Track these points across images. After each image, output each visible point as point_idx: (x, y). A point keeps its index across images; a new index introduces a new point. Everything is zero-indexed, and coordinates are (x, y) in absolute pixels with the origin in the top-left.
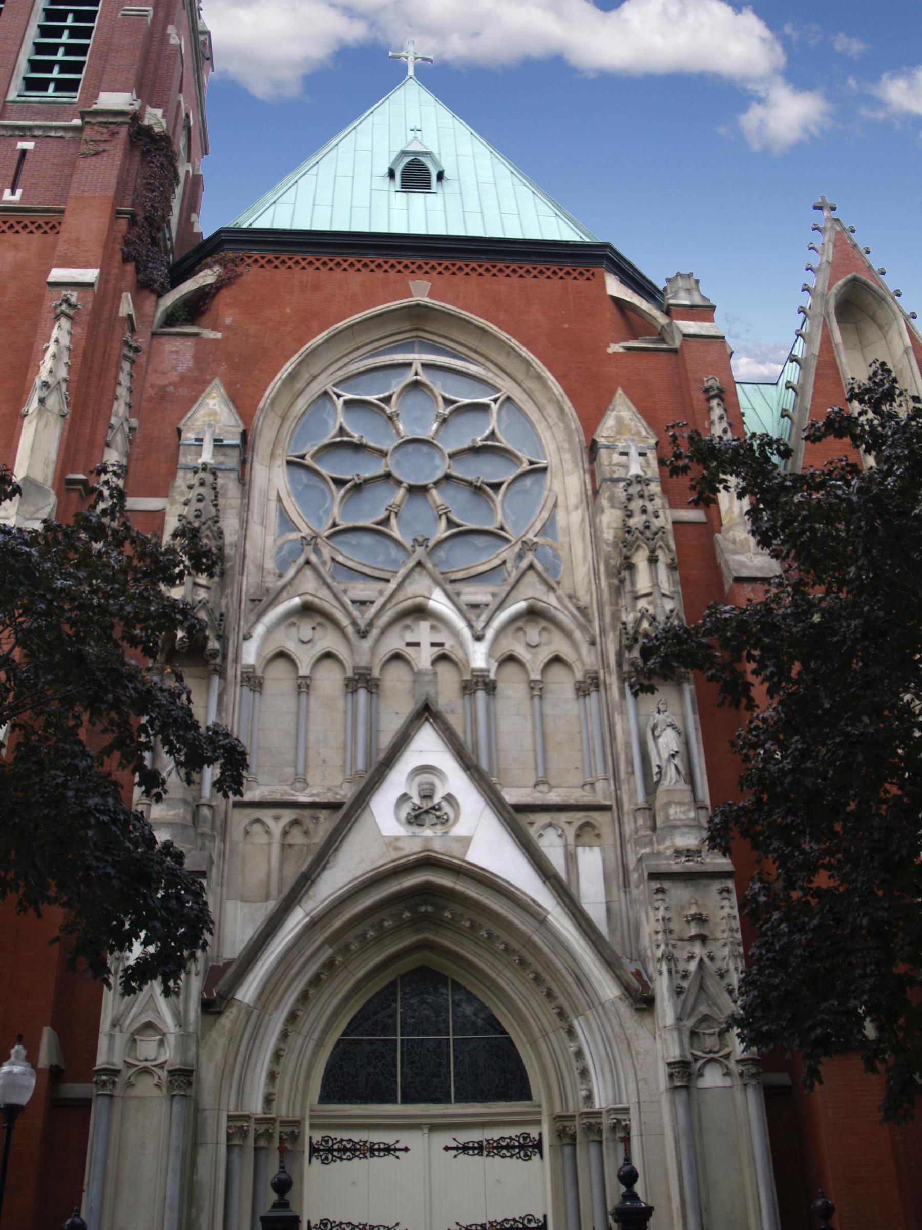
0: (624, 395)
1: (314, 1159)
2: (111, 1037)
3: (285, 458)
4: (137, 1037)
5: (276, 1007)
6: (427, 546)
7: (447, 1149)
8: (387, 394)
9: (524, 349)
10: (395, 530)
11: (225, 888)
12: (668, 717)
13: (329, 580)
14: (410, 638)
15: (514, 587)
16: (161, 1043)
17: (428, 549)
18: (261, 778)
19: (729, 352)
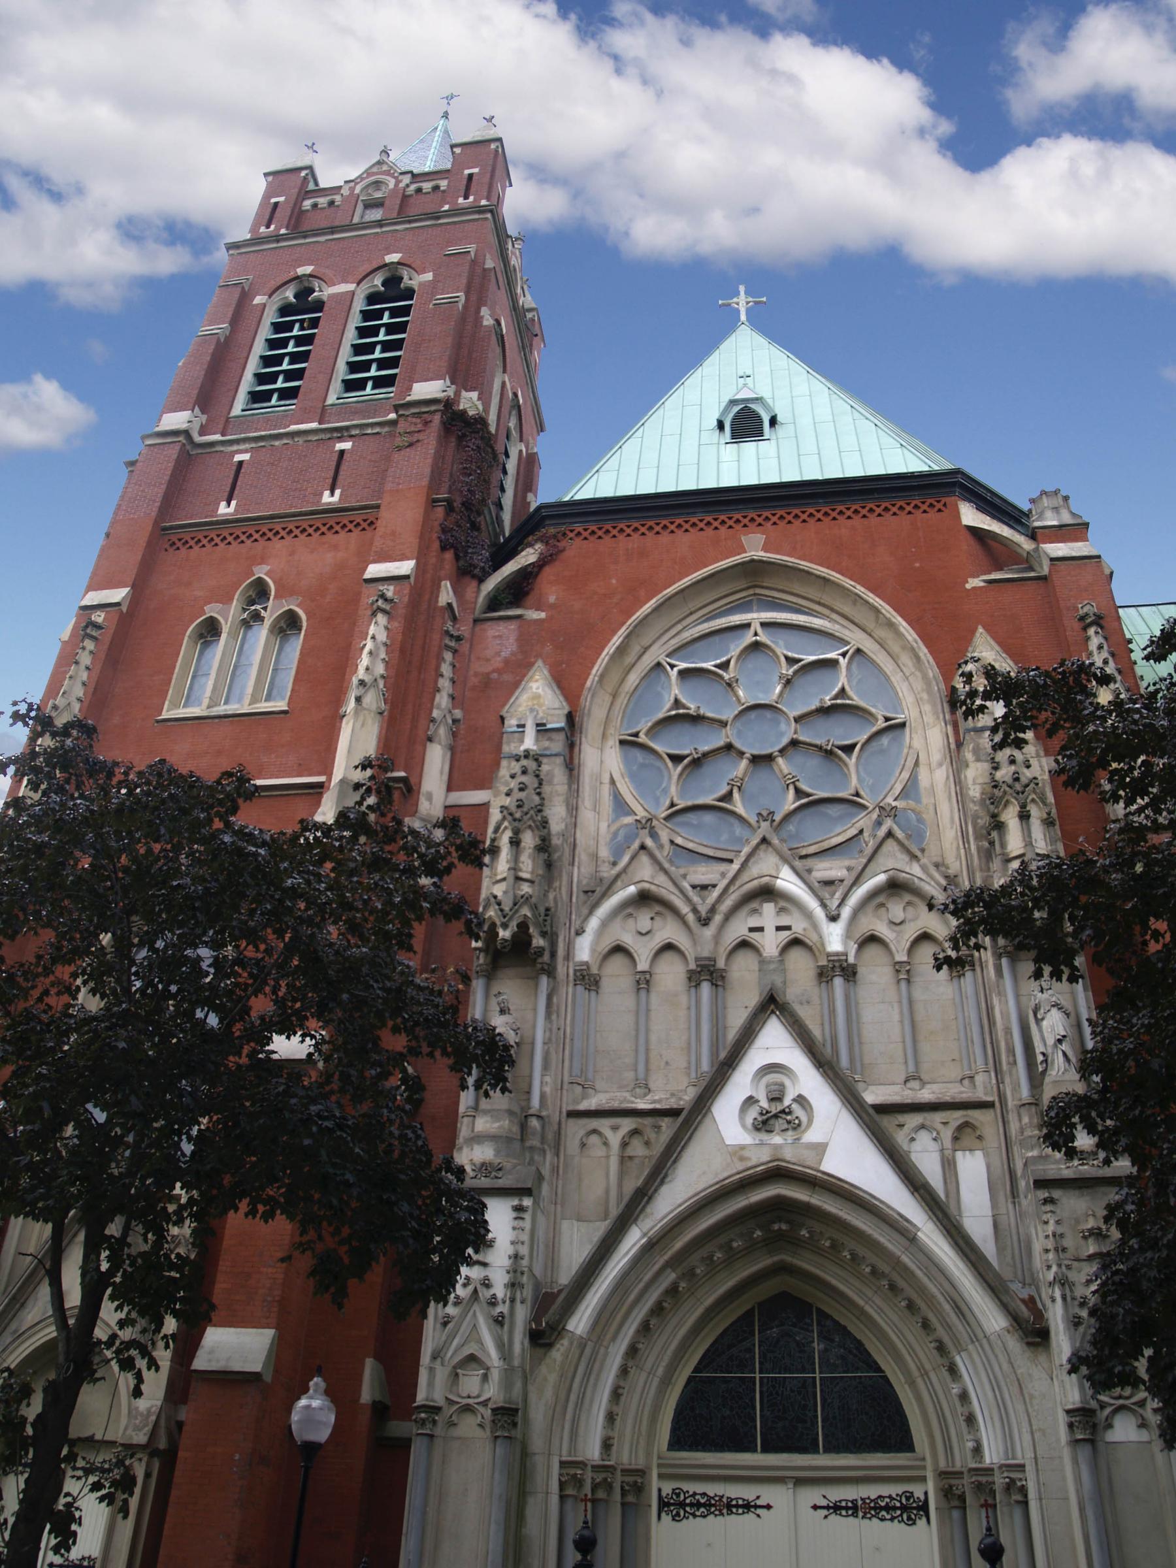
0: (985, 634)
1: (663, 1515)
2: (431, 1370)
3: (617, 738)
4: (459, 1371)
5: (614, 1338)
6: (773, 821)
7: (815, 1507)
8: (724, 659)
9: (871, 595)
10: (738, 806)
11: (559, 1207)
12: (1052, 995)
13: (666, 865)
14: (754, 922)
15: (869, 861)
16: (485, 1378)
17: (775, 824)
18: (599, 1085)
19: (1107, 572)
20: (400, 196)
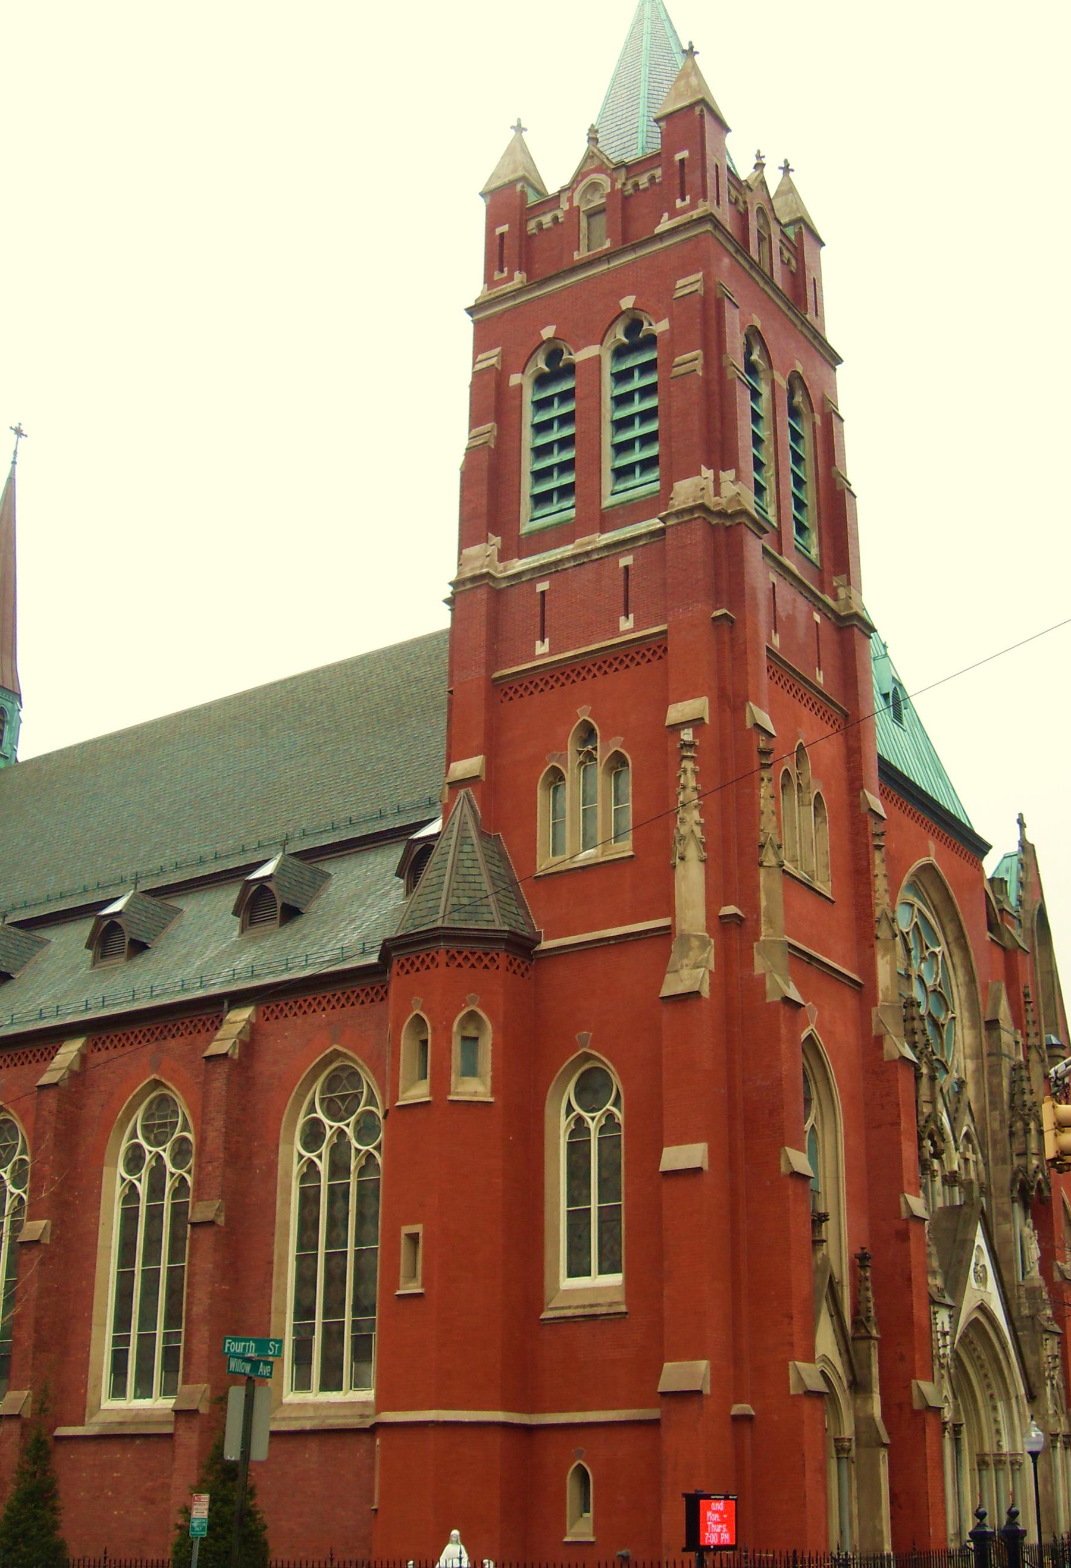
20: (619, 197)
